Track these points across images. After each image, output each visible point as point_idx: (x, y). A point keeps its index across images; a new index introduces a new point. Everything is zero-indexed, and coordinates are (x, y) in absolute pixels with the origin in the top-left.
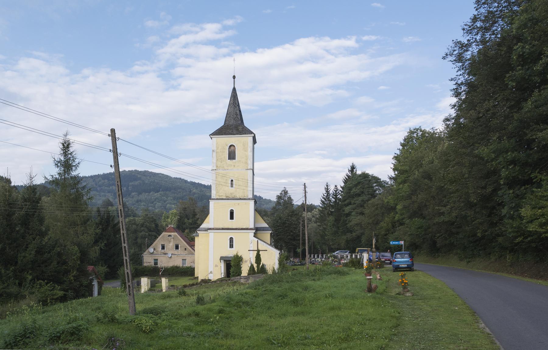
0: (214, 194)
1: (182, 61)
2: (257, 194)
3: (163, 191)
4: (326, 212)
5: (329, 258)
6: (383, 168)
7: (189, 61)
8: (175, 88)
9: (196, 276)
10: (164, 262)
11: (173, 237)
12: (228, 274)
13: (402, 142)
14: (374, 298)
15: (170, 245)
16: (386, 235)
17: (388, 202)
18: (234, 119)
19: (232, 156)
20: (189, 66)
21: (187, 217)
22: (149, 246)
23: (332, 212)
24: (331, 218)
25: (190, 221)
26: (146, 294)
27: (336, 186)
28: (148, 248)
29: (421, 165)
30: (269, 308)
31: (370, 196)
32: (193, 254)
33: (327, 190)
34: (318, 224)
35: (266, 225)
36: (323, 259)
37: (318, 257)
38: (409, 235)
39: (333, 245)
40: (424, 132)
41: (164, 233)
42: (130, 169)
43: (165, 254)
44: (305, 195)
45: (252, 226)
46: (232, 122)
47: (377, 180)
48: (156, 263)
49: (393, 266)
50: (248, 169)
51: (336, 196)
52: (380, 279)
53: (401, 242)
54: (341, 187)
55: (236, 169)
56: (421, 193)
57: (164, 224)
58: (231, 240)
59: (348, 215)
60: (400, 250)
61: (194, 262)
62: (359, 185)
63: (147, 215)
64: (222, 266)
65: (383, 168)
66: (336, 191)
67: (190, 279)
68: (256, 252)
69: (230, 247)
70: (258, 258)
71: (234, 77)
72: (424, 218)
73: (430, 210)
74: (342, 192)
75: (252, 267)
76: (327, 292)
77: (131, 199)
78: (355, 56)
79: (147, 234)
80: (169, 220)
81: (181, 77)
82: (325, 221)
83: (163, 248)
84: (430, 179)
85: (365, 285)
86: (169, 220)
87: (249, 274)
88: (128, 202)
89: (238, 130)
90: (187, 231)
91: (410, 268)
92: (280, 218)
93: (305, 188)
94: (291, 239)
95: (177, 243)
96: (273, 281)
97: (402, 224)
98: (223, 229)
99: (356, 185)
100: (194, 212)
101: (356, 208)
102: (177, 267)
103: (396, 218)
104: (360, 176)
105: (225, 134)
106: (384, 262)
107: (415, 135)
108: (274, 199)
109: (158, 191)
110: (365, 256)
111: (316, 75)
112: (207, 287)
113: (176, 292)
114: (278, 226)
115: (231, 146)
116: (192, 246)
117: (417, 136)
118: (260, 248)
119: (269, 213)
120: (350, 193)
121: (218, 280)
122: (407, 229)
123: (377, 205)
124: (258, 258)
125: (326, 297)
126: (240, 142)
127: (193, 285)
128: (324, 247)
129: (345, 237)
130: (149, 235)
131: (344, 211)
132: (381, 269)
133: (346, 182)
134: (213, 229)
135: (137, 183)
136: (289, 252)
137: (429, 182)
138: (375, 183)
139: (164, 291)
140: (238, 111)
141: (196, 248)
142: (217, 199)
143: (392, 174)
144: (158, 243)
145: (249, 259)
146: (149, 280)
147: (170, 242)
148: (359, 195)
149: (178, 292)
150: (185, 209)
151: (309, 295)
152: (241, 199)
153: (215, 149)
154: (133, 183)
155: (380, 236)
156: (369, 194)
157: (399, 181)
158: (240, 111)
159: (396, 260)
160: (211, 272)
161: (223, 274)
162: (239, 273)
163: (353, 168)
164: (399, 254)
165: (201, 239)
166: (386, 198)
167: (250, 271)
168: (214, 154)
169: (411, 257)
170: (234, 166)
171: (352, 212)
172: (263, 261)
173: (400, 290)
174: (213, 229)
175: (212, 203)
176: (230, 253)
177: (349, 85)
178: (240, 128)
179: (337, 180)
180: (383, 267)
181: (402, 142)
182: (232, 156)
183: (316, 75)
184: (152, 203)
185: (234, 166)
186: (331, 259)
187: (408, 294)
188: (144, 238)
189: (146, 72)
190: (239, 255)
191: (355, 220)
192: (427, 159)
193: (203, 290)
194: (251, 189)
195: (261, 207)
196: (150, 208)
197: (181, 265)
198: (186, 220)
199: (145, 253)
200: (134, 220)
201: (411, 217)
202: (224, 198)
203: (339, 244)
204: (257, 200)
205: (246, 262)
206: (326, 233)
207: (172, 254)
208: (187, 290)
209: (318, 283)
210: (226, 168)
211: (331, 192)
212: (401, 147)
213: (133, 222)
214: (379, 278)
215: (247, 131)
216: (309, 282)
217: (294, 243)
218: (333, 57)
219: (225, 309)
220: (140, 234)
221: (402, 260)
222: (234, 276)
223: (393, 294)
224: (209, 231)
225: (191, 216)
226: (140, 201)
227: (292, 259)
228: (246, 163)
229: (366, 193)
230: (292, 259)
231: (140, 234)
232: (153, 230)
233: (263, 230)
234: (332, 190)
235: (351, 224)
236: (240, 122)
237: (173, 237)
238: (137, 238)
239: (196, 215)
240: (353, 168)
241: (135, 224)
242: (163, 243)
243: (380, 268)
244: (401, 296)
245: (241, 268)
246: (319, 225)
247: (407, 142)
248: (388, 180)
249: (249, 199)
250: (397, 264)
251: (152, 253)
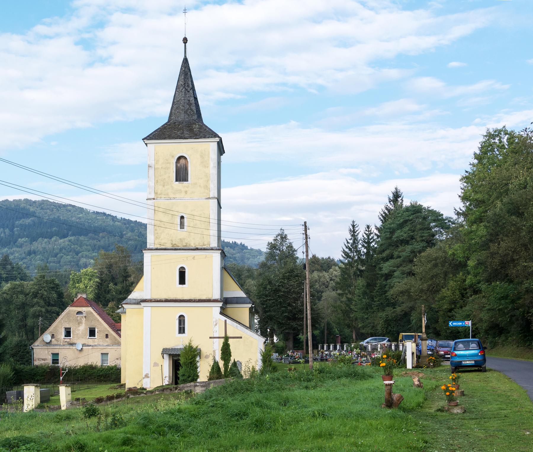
0: (151, 241)
1: (116, 17)
2: (226, 238)
3: (73, 235)
4: (352, 271)
5: (352, 351)
6: (445, 197)
7: (127, 18)
10: (70, 359)
11: (84, 315)
12: (176, 379)
13: (478, 152)
14: (394, 417)
15: (80, 330)
16: (450, 310)
17: (454, 254)
18: (186, 112)
19: (182, 175)
20: (129, 26)
21: (113, 279)
22: (44, 330)
23: (361, 271)
24: (361, 282)
25: (119, 287)
26: (31, 415)
27: (368, 227)
29: (507, 191)
30: (212, 436)
31: (424, 244)
33: (353, 232)
34: (339, 291)
35: (242, 294)
36: (343, 352)
37: (335, 348)
38: (489, 310)
39: (363, 327)
40: (512, 136)
41: (69, 309)
42: (17, 198)
43: (72, 344)
44: (307, 242)
46: (182, 117)
47: (436, 216)
48: (55, 361)
49: (451, 363)
50: (209, 198)
51: (369, 243)
52: (419, 386)
53: (467, 322)
54: (377, 228)
55: (192, 199)
56: (505, 238)
57: (74, 291)
58: (181, 319)
59: (388, 276)
60: (467, 336)
61: (119, 359)
62: (406, 224)
64: (166, 365)
65: (445, 197)
66: (368, 236)
67: (111, 388)
68: (222, 340)
70: (226, 351)
72: (511, 281)
73: (519, 268)
74: (378, 236)
75: (216, 366)
76: (316, 408)
77: (17, 249)
78: (408, 13)
79: (43, 310)
80: (82, 286)
81: (114, 43)
82: (350, 286)
83: (68, 333)
84: (520, 215)
85: (383, 395)
87: (210, 379)
88: (12, 254)
89: (191, 130)
90: (110, 305)
91: (479, 367)
92: (270, 283)
96: (236, 389)
97: (477, 292)
98: (167, 301)
99: (401, 226)
100: (125, 270)
101: (401, 265)
103: (468, 281)
104: (407, 209)
105: (170, 137)
106: (443, 357)
107: (497, 141)
108: (264, 249)
109: (65, 236)
110: (410, 347)
111: (344, 42)
112: (138, 402)
114: (266, 296)
115: (180, 158)
116: (118, 331)
117: (500, 142)
118: (229, 335)
120: (391, 238)
121: (157, 389)
122: (484, 300)
123: (436, 259)
124: (226, 351)
125: (314, 416)
126: (197, 152)
127: (119, 396)
128: (347, 331)
129: (382, 314)
130: (47, 311)
131: (381, 269)
132: (436, 369)
133: (385, 218)
134: (150, 301)
135: (28, 221)
137: (518, 220)
138: (434, 221)
139: (63, 408)
140: (192, 99)
141: (122, 333)
142: (157, 249)
143: (461, 206)
144: (59, 325)
145: (210, 353)
146: (38, 391)
147: (80, 323)
148: (405, 242)
150: (110, 267)
151: (285, 413)
152: (197, 249)
153: (152, 162)
154: (21, 222)
155: (441, 313)
156: (423, 240)
157: (472, 218)
158: (196, 99)
159: (456, 352)
160: (147, 376)
161: (167, 379)
162: (194, 377)
163: (397, 196)
164: (462, 342)
165: (130, 316)
166: (450, 247)
168: (152, 171)
169: (481, 347)
171: (395, 271)
172: (235, 356)
173: (443, 403)
174: (150, 301)
175: (147, 256)
176: (178, 342)
177: (402, 60)
178: (196, 127)
179: (370, 217)
180: (440, 365)
181: (478, 152)
182: (182, 175)
183: (344, 42)
184: (56, 256)
186: (355, 352)
187: (457, 410)
189: (57, 35)
191: (399, 284)
192: (516, 182)
193: (129, 406)
194: (216, 233)
195: (233, 262)
197: (99, 364)
198: (111, 285)
199: (36, 343)
200: (22, 286)
201: (489, 281)
202: (169, 246)
203: (373, 327)
204: (224, 249)
205: (207, 357)
206: (352, 307)
207: (84, 345)
208: (100, 407)
209: (312, 392)
210: (172, 196)
211: (360, 237)
212: (476, 161)
213: (19, 290)
214: (417, 383)
215: (206, 133)
216: (297, 392)
218: (372, 13)
219: (134, 438)
221: (467, 352)
222: (185, 381)
223: (432, 411)
224: (143, 304)
226: (35, 252)
227: (290, 353)
228: (207, 187)
229: (418, 239)
230: (290, 353)
232: (56, 301)
233: (237, 303)
234: (361, 235)
235: (392, 292)
236: (195, 117)
237: (84, 315)
238: (25, 317)
239: (129, 276)
240: (397, 196)
241: (22, 292)
242: (68, 326)
243: (434, 366)
244: (444, 414)
245: (197, 368)
246: (339, 294)
247: (485, 155)
248: (455, 217)
250: (457, 359)
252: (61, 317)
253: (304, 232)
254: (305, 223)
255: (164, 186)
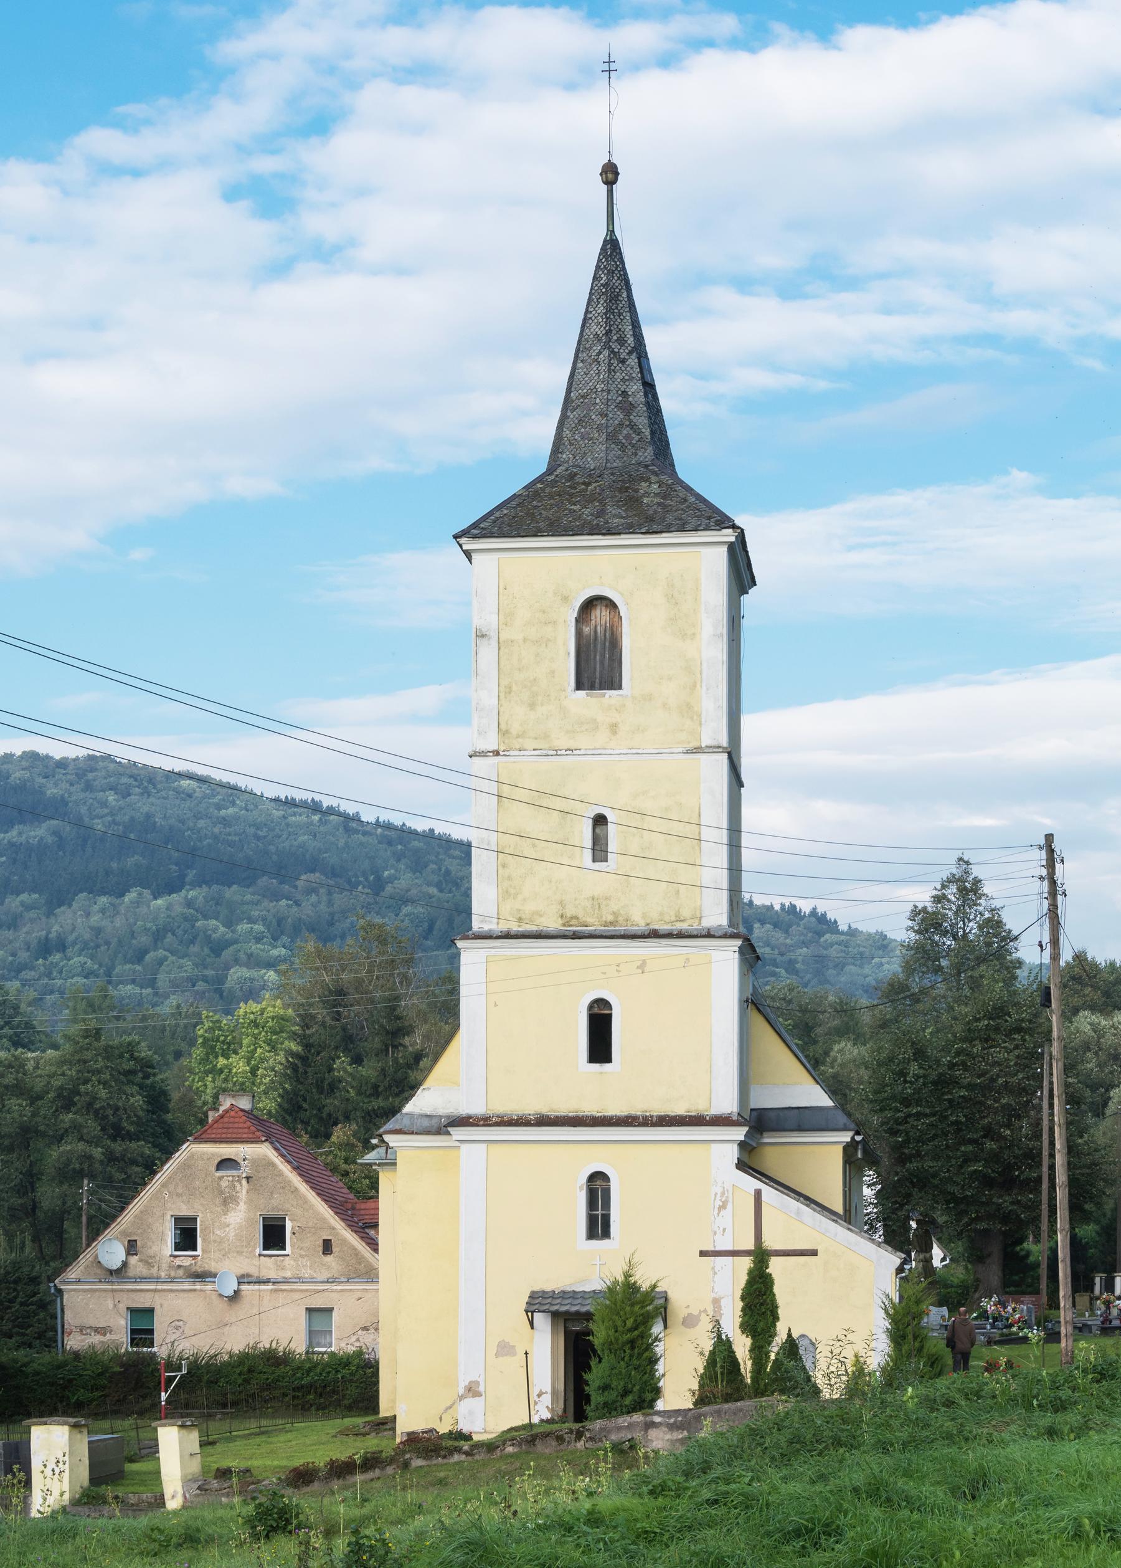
1: (374, 97)
2: (760, 893)
7: (414, 99)
8: (329, 255)
9: (384, 1411)
10: (194, 1328)
11: (245, 1171)
12: (578, 1400)
15: (231, 1226)
18: (612, 437)
19: (598, 664)
21: (348, 1041)
22: (99, 1224)
25: (368, 1071)
28: (95, 1233)
32: (370, 1275)
41: (190, 1150)
43: (202, 1276)
45: (727, 1103)
46: (597, 454)
48: (142, 1334)
50: (698, 750)
55: (638, 752)
58: (598, 1188)
61: (372, 1327)
63: (98, 1033)
64: (543, 1348)
67: (345, 1433)
69: (592, 1234)
71: (610, 174)
75: (723, 1350)
83: (187, 1237)
86: (239, 1066)
87: (703, 1400)
89: (632, 502)
90: (339, 1134)
92: (919, 1054)
93: (1051, 865)
94: (988, 1182)
95: (275, 1205)
96: (796, 1440)
100: (392, 1011)
102: (273, 1359)
105: (556, 529)
112: (442, 1483)
113: (235, 1507)
114: (906, 1102)
115: (590, 604)
116: (366, 1227)
118: (771, 1241)
119: (866, 1018)
121: (511, 1436)
126: (657, 580)
127: (370, 1462)
130: (111, 1158)
134: (485, 1121)
135: (39, 833)
136: (976, 1256)
139: (173, 1504)
140: (636, 387)
141: (384, 1235)
142: (507, 936)
144: (155, 1207)
145: (703, 1307)
147: (228, 1201)
149: (250, 1510)
150: (337, 996)
152: (655, 935)
158: (649, 387)
160: (472, 1390)
162: (643, 1393)
165: (412, 1177)
167: (709, 1377)
170: (614, 728)
172: (792, 1319)
174: (485, 1121)
175: (474, 963)
178: (650, 491)
182: (598, 664)
185: (614, 728)
188: (70, 1175)
189: (165, 165)
190: (644, 1279)
193: (411, 1496)
196: (128, 989)
197: (299, 1346)
198: (342, 1064)
199: (73, 1273)
202: (553, 924)
205: (690, 1322)
207: (243, 1279)
209: (1069, 1449)
215: (694, 514)
217: (1005, 1201)
220: (55, 1154)
222: (610, 1410)
224: (459, 1133)
225: (377, 1042)
227: (990, 1305)
228: (689, 710)
231: (55, 1154)
232: (136, 1121)
233: (800, 1129)
237: (245, 1171)
238: (30, 1179)
239: (408, 1031)
242: (185, 1211)
245: (653, 1361)
249: (709, 935)
251: (119, 1273)
252: (160, 1178)
253: (1044, 872)
254: (1049, 838)
255: (532, 706)
